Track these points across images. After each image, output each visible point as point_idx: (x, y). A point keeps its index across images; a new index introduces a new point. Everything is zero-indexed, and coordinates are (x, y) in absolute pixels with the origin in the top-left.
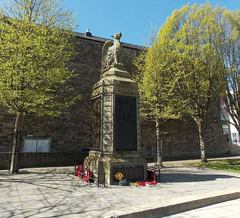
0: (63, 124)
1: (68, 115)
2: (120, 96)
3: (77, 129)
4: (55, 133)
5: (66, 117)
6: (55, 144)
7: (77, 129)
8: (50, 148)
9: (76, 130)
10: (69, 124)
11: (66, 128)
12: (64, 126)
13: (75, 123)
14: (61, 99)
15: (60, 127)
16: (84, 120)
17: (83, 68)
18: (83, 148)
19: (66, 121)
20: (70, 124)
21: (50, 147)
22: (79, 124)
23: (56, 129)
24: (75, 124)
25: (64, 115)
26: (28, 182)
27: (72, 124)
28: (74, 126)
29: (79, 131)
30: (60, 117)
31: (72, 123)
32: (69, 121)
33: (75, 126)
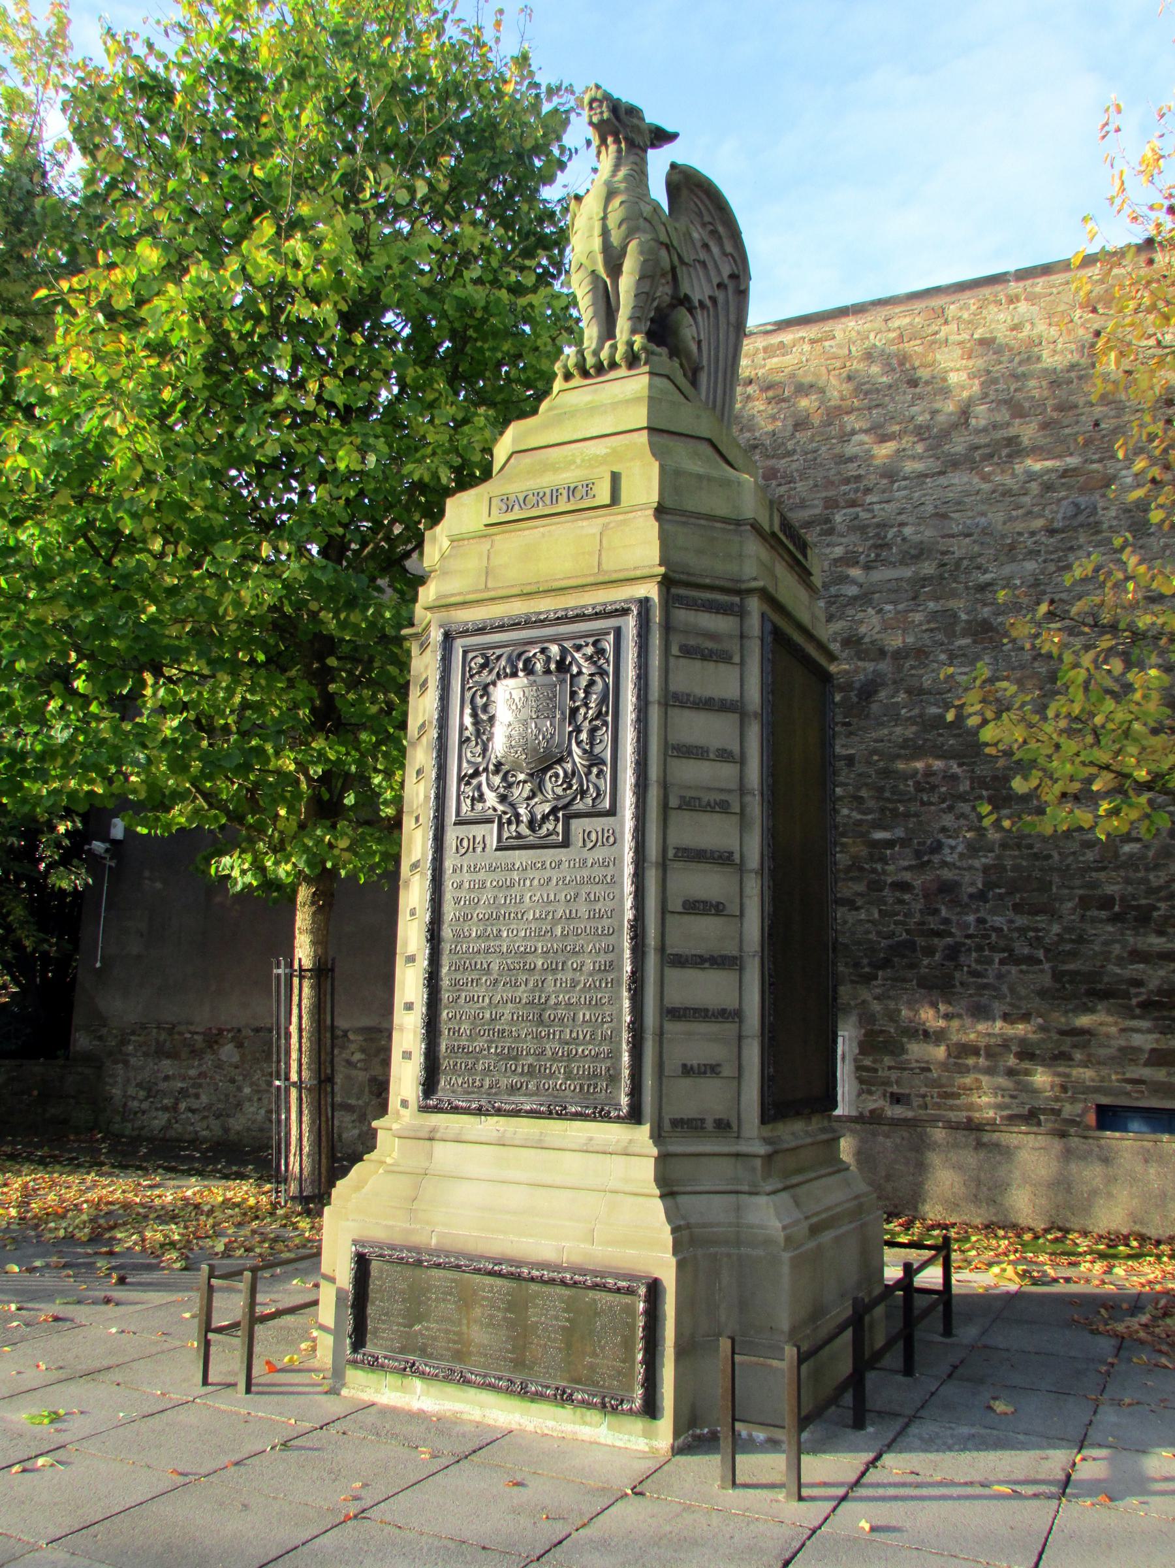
0: (933, 923)
1: (961, 855)
2: (499, 1112)
3: (1041, 954)
4: (878, 991)
5: (947, 874)
6: (888, 1061)
7: (1041, 954)
8: (855, 1093)
9: (1032, 960)
10: (971, 918)
11: (953, 953)
12: (939, 934)
13: (1017, 908)
14: (902, 748)
15: (910, 945)
16: (1094, 885)
17: (1048, 487)
18: (1105, 1100)
19: (955, 903)
20: (981, 921)
21: (855, 1083)
22: (1055, 915)
23: (886, 964)
24: (1021, 921)
25: (936, 859)
26: (731, 350)
27: (998, 920)
28: (1018, 929)
29: (1053, 969)
30: (907, 876)
31: (993, 912)
32: (971, 896)
33: (1022, 931)
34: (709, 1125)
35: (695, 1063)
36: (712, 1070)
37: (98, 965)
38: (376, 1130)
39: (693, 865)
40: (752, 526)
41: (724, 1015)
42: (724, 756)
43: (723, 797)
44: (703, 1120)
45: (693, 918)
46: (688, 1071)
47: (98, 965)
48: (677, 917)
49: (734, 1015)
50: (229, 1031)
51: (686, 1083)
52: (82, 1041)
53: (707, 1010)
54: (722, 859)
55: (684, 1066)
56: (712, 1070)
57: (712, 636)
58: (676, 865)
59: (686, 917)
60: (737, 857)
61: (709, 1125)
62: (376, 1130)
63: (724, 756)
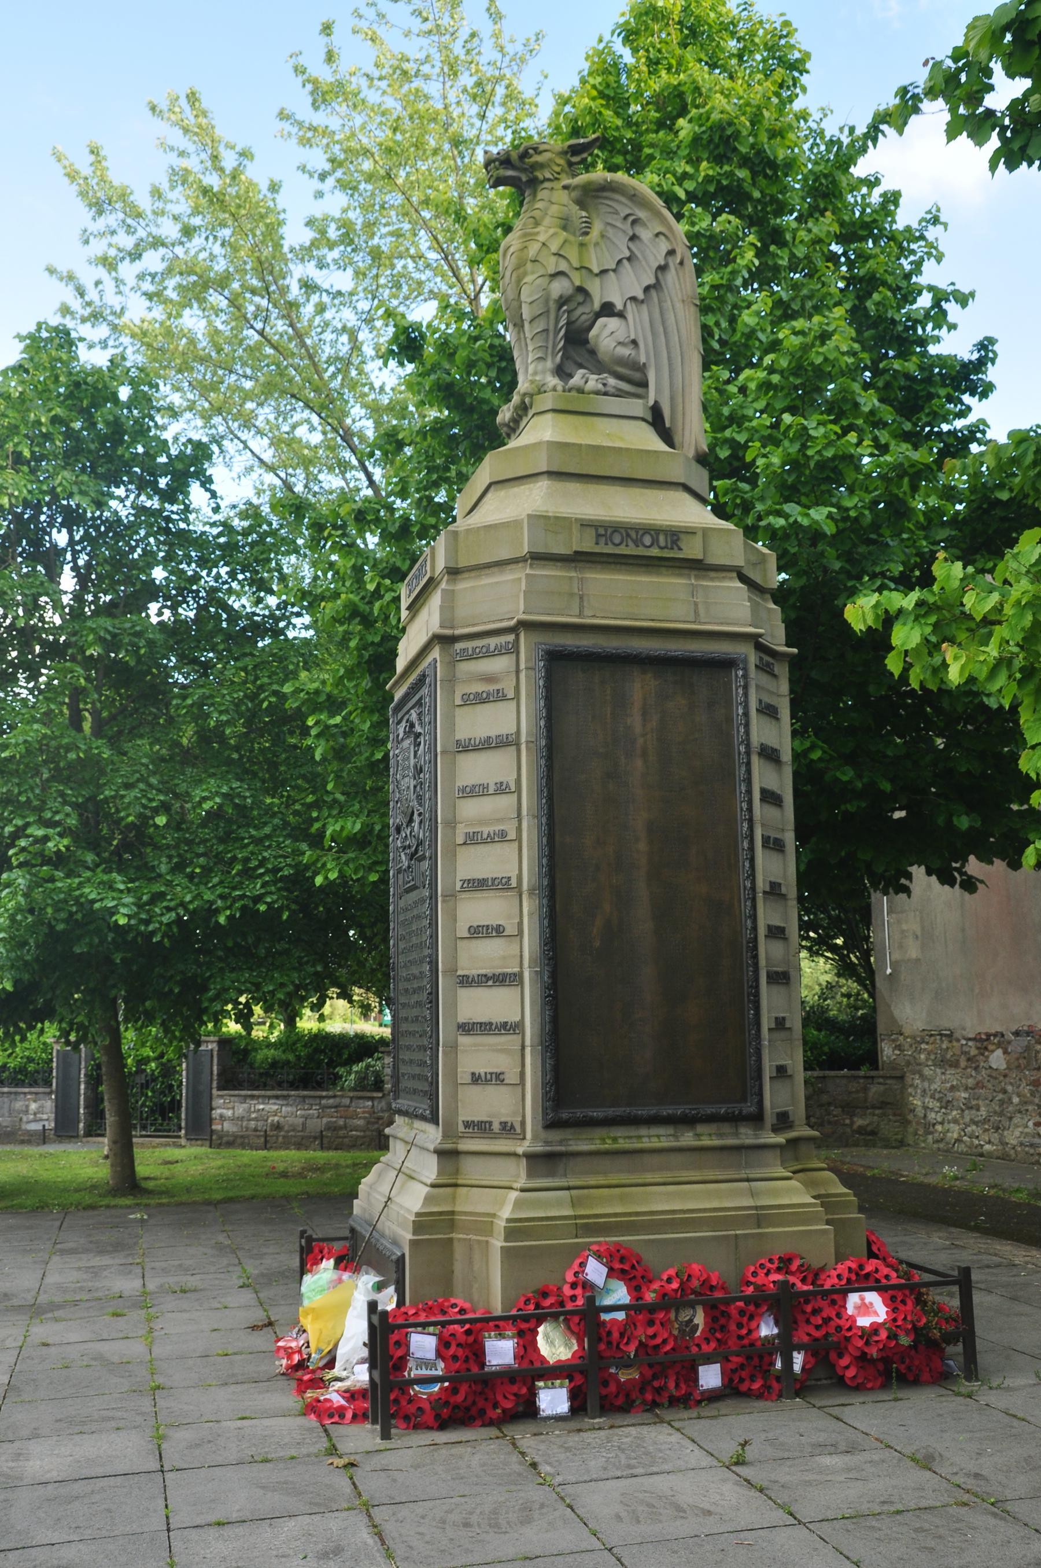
34: (496, 1127)
35: (482, 1071)
36: (498, 1078)
37: (889, 971)
38: (387, 1137)
39: (478, 895)
40: (532, 558)
41: (505, 1028)
42: (501, 789)
43: (498, 828)
44: (490, 1123)
45: (478, 942)
46: (476, 1079)
47: (889, 971)
48: (466, 941)
49: (513, 1028)
50: (995, 1035)
51: (476, 1089)
52: (887, 1051)
53: (491, 1024)
54: (501, 885)
55: (473, 1074)
56: (498, 1078)
57: (489, 679)
58: (464, 895)
59: (474, 941)
60: (514, 883)
61: (496, 1127)
62: (387, 1137)
63: (501, 789)
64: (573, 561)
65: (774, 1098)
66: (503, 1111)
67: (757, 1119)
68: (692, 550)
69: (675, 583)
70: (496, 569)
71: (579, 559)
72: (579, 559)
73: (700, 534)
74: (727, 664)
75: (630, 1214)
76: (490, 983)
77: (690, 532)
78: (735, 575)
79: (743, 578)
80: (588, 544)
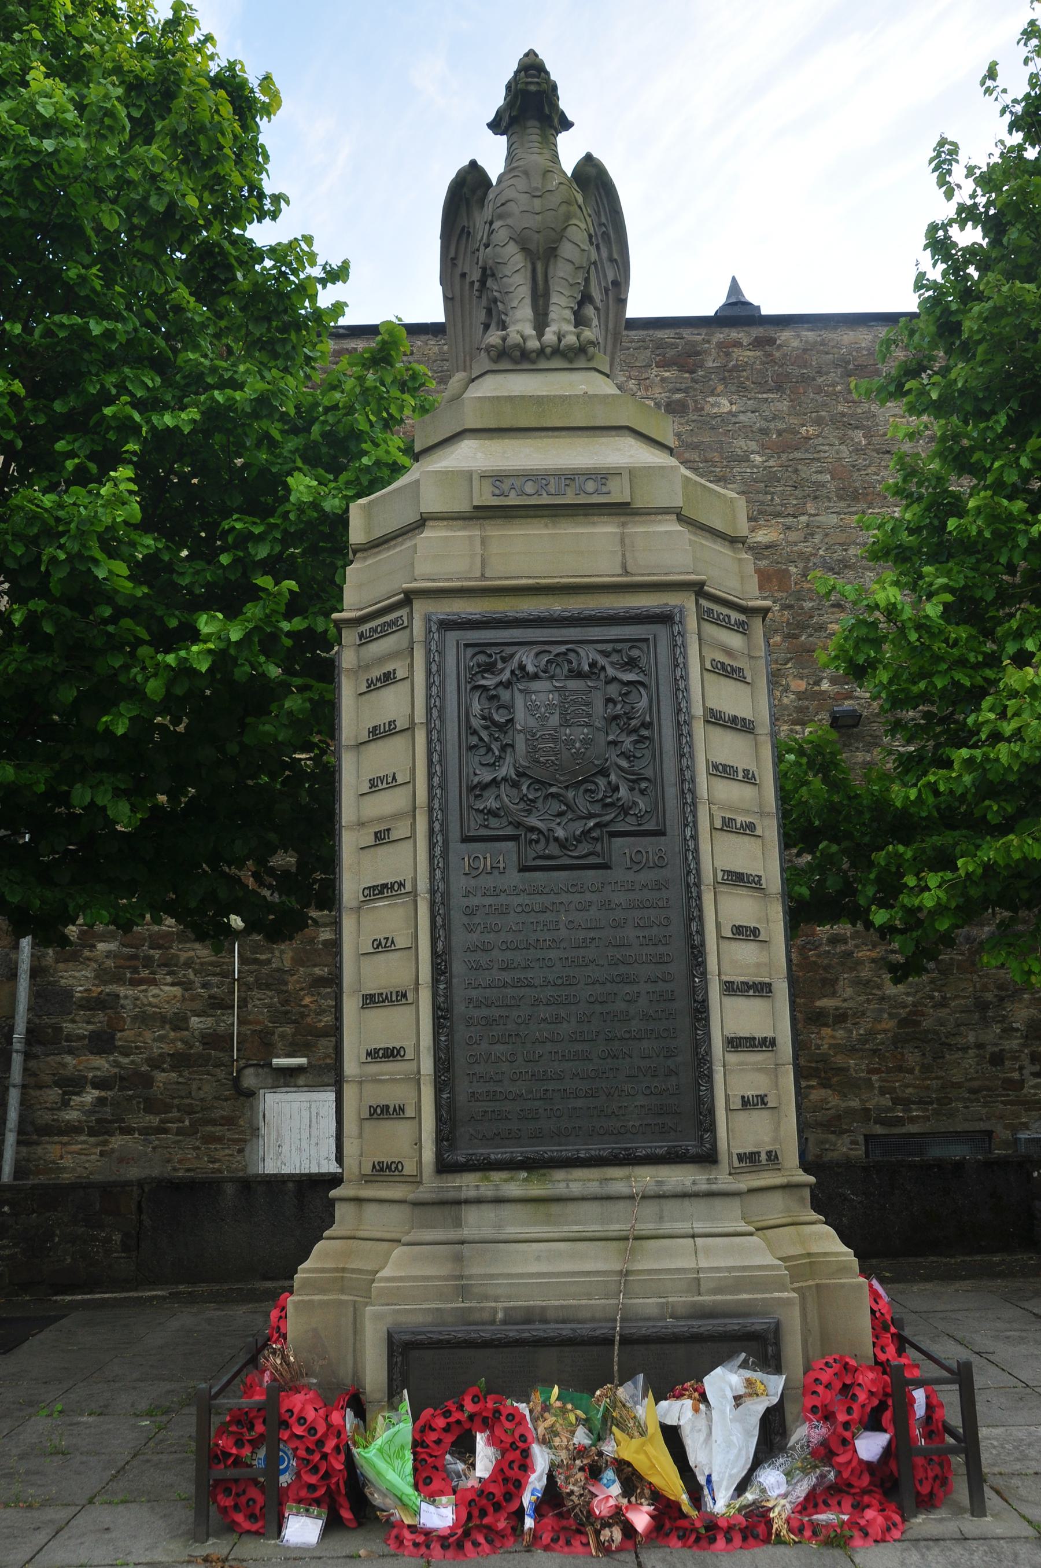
36: (761, 1101)
44: (759, 1153)
55: (743, 1097)
64: (471, 519)
65: (736, 1132)
66: (766, 1139)
67: (708, 1158)
68: (619, 492)
69: (606, 529)
70: (708, 535)
71: (482, 514)
72: (482, 514)
73: (626, 477)
74: (665, 618)
75: (744, 1268)
76: (751, 993)
77: (615, 473)
78: (674, 517)
79: (681, 518)
80: (485, 497)
